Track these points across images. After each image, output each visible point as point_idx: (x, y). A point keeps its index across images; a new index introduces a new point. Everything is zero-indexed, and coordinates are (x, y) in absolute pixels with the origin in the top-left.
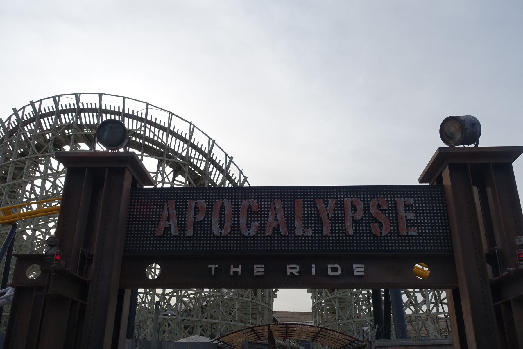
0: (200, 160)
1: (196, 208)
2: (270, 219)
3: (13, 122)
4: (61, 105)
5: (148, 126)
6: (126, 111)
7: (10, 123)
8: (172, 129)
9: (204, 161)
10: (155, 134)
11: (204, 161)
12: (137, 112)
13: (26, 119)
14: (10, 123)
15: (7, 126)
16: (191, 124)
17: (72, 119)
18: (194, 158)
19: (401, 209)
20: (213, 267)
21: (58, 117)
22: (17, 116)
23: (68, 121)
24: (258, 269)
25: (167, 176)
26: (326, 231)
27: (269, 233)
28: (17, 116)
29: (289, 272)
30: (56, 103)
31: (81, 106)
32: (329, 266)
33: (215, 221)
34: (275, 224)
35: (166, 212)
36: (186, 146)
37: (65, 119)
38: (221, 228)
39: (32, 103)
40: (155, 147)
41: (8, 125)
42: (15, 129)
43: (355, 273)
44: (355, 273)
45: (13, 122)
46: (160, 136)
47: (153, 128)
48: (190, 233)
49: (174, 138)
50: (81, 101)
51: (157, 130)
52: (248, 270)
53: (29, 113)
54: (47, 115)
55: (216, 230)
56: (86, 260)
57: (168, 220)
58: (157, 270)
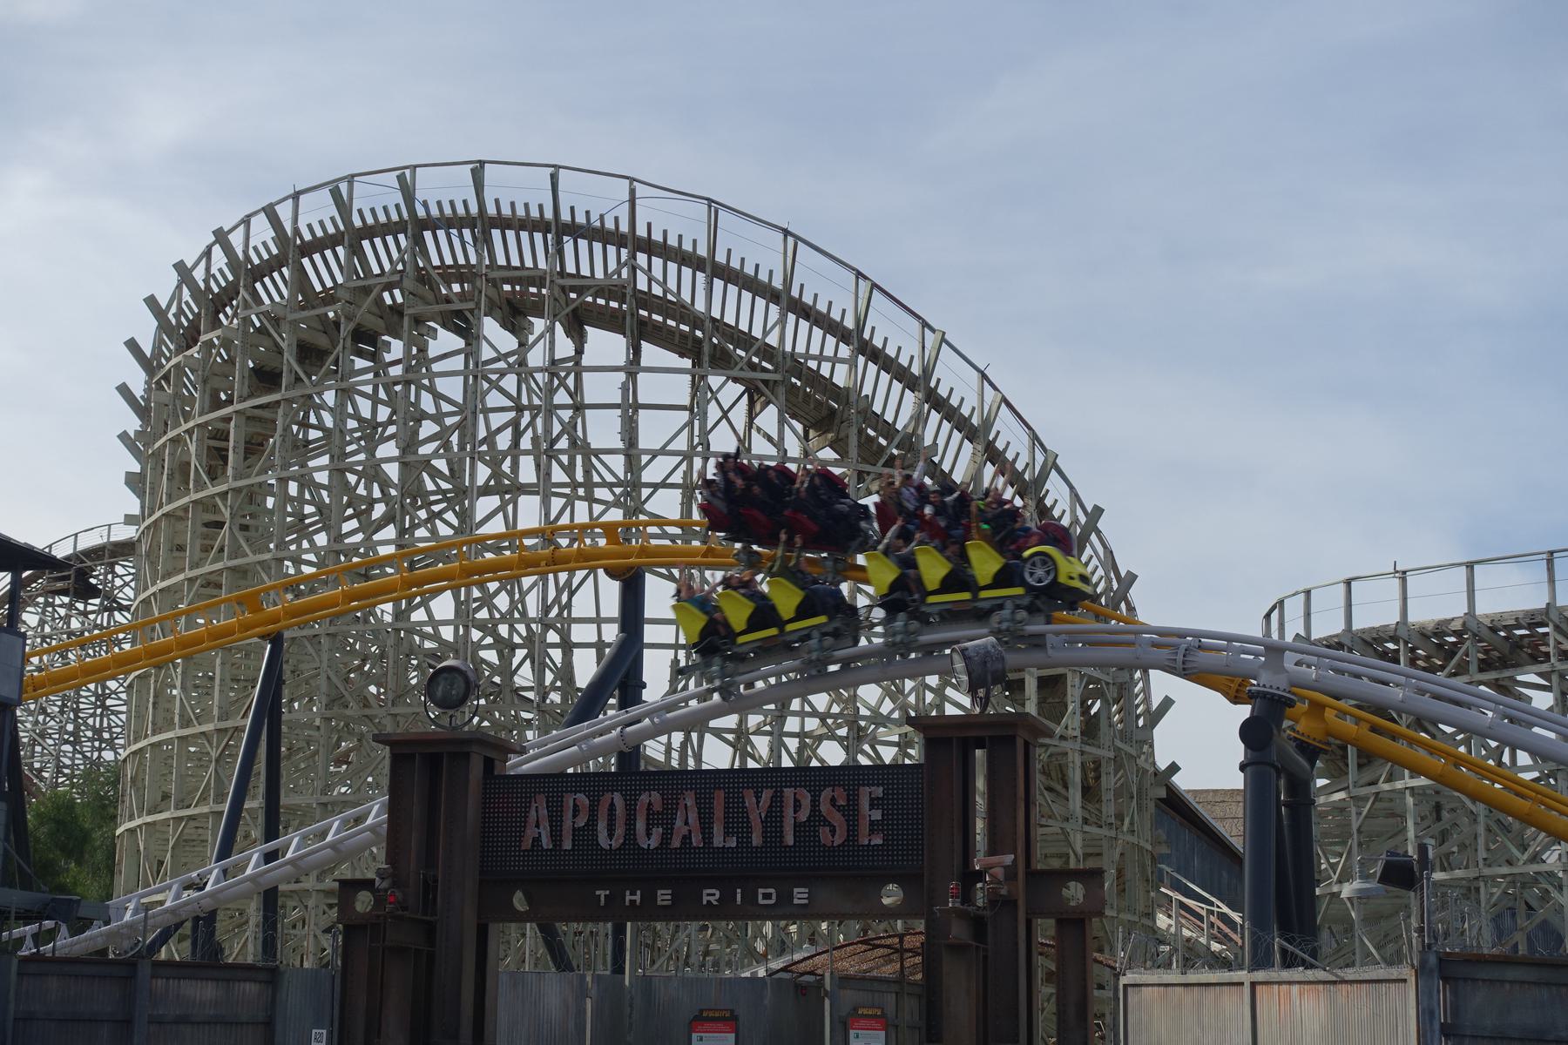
0: (827, 359)
1: (575, 805)
2: (679, 823)
3: (221, 271)
4: (360, 211)
5: (642, 259)
7: (180, 312)
8: (721, 258)
12: (602, 217)
13: (256, 261)
15: (202, 285)
16: (786, 233)
17: (402, 260)
19: (865, 803)
21: (354, 253)
22: (228, 250)
23: (387, 267)
24: (664, 896)
25: (725, 415)
26: (756, 840)
27: (676, 843)
28: (228, 250)
29: (705, 899)
30: (343, 206)
31: (421, 213)
32: (761, 891)
33: (602, 826)
34: (685, 830)
35: (533, 813)
36: (774, 310)
37: (381, 256)
38: (611, 836)
39: (221, 237)
41: (206, 281)
42: (230, 293)
43: (796, 901)
44: (796, 901)
45: (221, 271)
46: (672, 285)
48: (567, 845)
49: (733, 290)
50: (420, 195)
52: (649, 898)
53: (264, 244)
56: (429, 887)
57: (538, 826)
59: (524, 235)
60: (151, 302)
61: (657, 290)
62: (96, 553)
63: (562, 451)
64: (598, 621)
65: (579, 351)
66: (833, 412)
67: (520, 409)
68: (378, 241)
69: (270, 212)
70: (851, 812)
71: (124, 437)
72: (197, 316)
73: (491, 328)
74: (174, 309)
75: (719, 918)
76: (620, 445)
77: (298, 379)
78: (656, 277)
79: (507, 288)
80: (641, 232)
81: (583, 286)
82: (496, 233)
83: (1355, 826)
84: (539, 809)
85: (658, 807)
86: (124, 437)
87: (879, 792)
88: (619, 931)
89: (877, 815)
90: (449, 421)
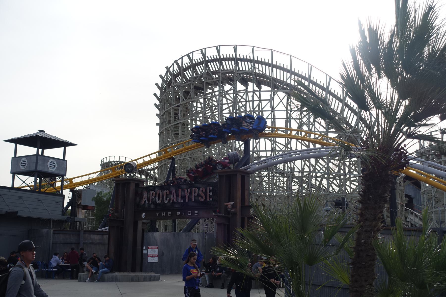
2: (172, 197)
5: (256, 65)
8: (274, 63)
12: (246, 56)
19: (208, 191)
20: (158, 213)
26: (187, 200)
27: (171, 202)
36: (289, 74)
37: (200, 69)
38: (159, 200)
39: (176, 62)
46: (260, 69)
48: (151, 203)
49: (278, 70)
52: (167, 214)
54: (187, 69)
55: (157, 201)
59: (227, 62)
60: (161, 76)
61: (261, 73)
63: (257, 111)
64: (266, 151)
65: (247, 88)
67: (246, 102)
68: (199, 66)
70: (205, 193)
71: (155, 105)
73: (239, 84)
74: (166, 77)
75: (180, 218)
76: (271, 109)
77: (184, 100)
79: (227, 75)
80: (256, 59)
81: (243, 72)
82: (224, 62)
83: (433, 195)
84: (145, 195)
85: (168, 193)
86: (155, 105)
87: (211, 188)
88: (174, 222)
89: (211, 194)
90: (230, 105)
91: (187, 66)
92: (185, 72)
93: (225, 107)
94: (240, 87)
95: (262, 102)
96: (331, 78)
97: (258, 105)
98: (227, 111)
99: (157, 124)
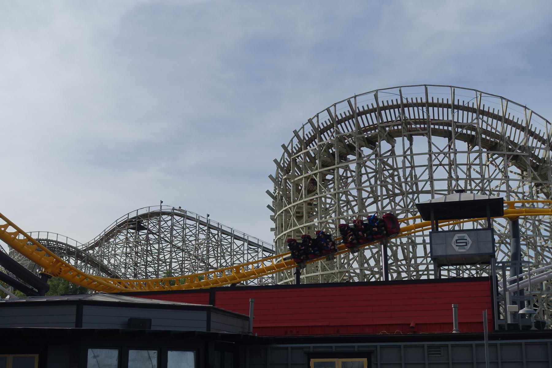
3: (297, 145)
6: (456, 103)
7: (284, 161)
9: (543, 149)
10: (488, 124)
11: (543, 149)
14: (284, 161)
18: (536, 148)
23: (470, 121)
40: (488, 138)
41: (292, 149)
45: (297, 145)
46: (494, 126)
47: (485, 118)
51: (490, 119)
53: (309, 132)
54: (365, 113)
58: (425, 234)
60: (275, 161)
61: (493, 131)
62: (145, 216)
66: (496, 143)
69: (328, 110)
72: (290, 162)
74: (282, 162)
78: (435, 114)
90: (370, 175)
91: (325, 125)
92: (322, 136)
93: (364, 178)
94: (385, 146)
95: (402, 154)
96: (532, 112)
97: (411, 174)
98: (367, 184)
99: (272, 229)
